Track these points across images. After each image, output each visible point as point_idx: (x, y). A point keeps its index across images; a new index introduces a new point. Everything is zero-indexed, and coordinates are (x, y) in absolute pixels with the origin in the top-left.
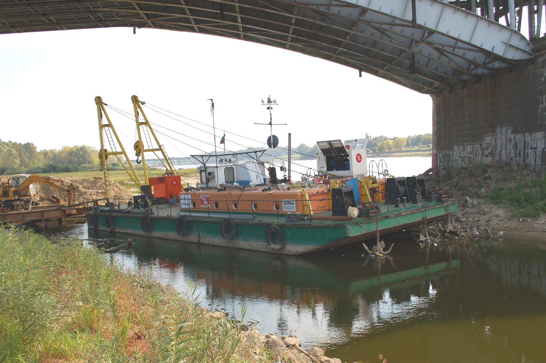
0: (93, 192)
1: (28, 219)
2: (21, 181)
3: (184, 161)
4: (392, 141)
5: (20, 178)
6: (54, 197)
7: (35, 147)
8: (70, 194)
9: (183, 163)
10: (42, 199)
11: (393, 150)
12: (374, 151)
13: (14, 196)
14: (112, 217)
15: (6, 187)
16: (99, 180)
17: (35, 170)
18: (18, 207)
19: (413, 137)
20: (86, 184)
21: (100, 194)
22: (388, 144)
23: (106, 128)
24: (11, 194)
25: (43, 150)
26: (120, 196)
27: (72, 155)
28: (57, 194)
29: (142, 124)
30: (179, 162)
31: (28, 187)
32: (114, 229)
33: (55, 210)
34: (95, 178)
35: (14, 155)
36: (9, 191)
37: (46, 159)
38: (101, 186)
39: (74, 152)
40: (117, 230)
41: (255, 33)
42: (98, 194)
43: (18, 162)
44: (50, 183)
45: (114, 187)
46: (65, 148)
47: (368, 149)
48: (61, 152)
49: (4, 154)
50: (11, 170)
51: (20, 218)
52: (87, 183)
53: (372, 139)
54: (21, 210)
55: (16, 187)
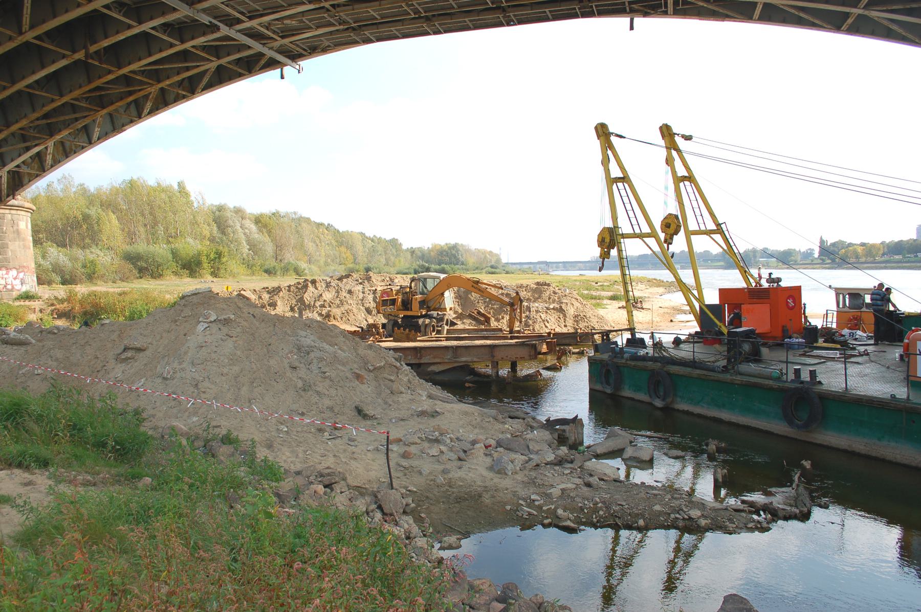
1: (464, 359)
2: (430, 285)
3: (571, 266)
4: (862, 248)
8: (514, 310)
10: (460, 317)
11: (863, 260)
12: (833, 261)
14: (669, 374)
15: (406, 293)
16: (546, 287)
18: (427, 329)
19: (889, 242)
20: (525, 293)
21: (553, 311)
22: (855, 251)
23: (620, 185)
24: (415, 305)
26: (584, 316)
27: (442, 254)
29: (683, 181)
31: (443, 294)
33: (516, 345)
34: (538, 284)
38: (549, 298)
39: (445, 251)
40: (683, 406)
41: (894, 7)
42: (548, 311)
43: (383, 261)
45: (573, 299)
47: (824, 258)
48: (430, 251)
51: (449, 357)
52: (526, 291)
53: (829, 244)
54: (431, 334)
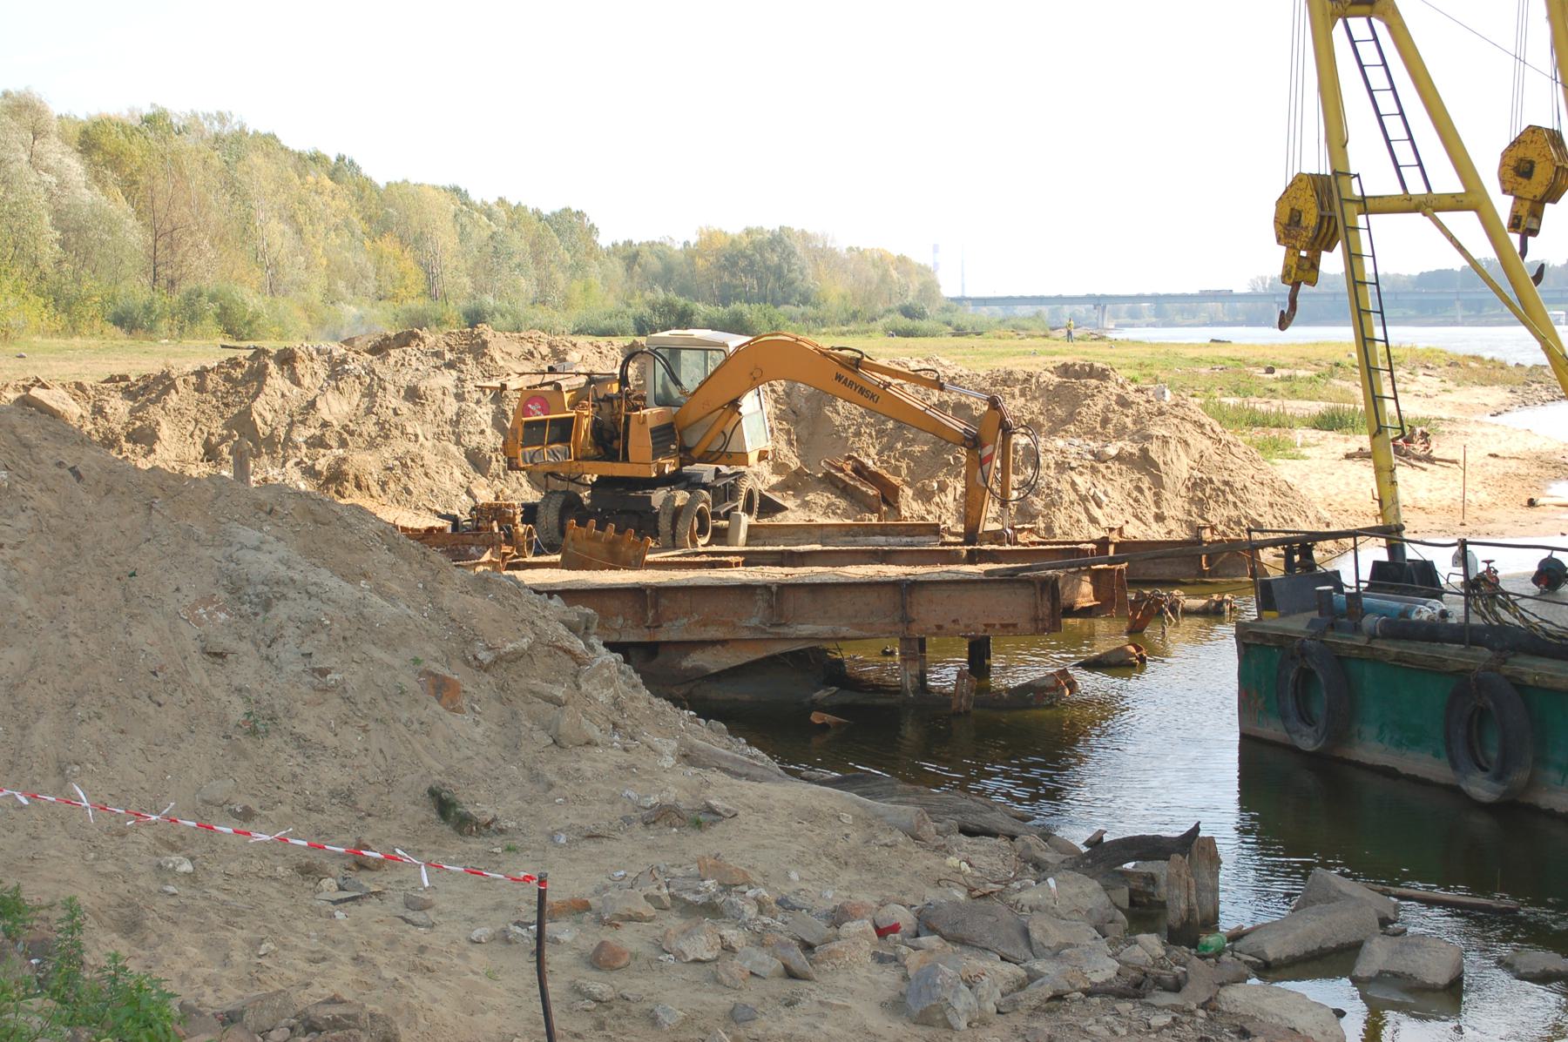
0: (1073, 450)
2: (692, 372)
5: (683, 353)
6: (860, 470)
7: (592, 226)
9: (1178, 319)
13: (655, 457)
14: (1520, 687)
15: (609, 399)
17: (607, 322)
18: (680, 526)
21: (1115, 466)
24: (640, 444)
25: (621, 244)
26: (1226, 483)
27: (735, 264)
28: (872, 452)
30: (1160, 314)
31: (734, 405)
32: (1531, 784)
33: (988, 581)
34: (1065, 370)
35: (511, 255)
36: (627, 424)
37: (632, 278)
39: (742, 254)
42: (1101, 467)
43: (527, 285)
44: (862, 391)
45: (1189, 426)
46: (709, 237)
48: (691, 253)
49: (476, 253)
50: (509, 318)
51: (754, 622)
52: (1023, 394)
54: (694, 543)
55: (664, 401)
